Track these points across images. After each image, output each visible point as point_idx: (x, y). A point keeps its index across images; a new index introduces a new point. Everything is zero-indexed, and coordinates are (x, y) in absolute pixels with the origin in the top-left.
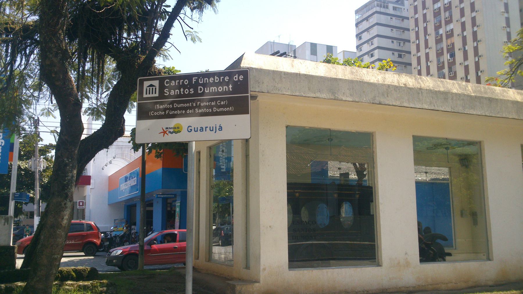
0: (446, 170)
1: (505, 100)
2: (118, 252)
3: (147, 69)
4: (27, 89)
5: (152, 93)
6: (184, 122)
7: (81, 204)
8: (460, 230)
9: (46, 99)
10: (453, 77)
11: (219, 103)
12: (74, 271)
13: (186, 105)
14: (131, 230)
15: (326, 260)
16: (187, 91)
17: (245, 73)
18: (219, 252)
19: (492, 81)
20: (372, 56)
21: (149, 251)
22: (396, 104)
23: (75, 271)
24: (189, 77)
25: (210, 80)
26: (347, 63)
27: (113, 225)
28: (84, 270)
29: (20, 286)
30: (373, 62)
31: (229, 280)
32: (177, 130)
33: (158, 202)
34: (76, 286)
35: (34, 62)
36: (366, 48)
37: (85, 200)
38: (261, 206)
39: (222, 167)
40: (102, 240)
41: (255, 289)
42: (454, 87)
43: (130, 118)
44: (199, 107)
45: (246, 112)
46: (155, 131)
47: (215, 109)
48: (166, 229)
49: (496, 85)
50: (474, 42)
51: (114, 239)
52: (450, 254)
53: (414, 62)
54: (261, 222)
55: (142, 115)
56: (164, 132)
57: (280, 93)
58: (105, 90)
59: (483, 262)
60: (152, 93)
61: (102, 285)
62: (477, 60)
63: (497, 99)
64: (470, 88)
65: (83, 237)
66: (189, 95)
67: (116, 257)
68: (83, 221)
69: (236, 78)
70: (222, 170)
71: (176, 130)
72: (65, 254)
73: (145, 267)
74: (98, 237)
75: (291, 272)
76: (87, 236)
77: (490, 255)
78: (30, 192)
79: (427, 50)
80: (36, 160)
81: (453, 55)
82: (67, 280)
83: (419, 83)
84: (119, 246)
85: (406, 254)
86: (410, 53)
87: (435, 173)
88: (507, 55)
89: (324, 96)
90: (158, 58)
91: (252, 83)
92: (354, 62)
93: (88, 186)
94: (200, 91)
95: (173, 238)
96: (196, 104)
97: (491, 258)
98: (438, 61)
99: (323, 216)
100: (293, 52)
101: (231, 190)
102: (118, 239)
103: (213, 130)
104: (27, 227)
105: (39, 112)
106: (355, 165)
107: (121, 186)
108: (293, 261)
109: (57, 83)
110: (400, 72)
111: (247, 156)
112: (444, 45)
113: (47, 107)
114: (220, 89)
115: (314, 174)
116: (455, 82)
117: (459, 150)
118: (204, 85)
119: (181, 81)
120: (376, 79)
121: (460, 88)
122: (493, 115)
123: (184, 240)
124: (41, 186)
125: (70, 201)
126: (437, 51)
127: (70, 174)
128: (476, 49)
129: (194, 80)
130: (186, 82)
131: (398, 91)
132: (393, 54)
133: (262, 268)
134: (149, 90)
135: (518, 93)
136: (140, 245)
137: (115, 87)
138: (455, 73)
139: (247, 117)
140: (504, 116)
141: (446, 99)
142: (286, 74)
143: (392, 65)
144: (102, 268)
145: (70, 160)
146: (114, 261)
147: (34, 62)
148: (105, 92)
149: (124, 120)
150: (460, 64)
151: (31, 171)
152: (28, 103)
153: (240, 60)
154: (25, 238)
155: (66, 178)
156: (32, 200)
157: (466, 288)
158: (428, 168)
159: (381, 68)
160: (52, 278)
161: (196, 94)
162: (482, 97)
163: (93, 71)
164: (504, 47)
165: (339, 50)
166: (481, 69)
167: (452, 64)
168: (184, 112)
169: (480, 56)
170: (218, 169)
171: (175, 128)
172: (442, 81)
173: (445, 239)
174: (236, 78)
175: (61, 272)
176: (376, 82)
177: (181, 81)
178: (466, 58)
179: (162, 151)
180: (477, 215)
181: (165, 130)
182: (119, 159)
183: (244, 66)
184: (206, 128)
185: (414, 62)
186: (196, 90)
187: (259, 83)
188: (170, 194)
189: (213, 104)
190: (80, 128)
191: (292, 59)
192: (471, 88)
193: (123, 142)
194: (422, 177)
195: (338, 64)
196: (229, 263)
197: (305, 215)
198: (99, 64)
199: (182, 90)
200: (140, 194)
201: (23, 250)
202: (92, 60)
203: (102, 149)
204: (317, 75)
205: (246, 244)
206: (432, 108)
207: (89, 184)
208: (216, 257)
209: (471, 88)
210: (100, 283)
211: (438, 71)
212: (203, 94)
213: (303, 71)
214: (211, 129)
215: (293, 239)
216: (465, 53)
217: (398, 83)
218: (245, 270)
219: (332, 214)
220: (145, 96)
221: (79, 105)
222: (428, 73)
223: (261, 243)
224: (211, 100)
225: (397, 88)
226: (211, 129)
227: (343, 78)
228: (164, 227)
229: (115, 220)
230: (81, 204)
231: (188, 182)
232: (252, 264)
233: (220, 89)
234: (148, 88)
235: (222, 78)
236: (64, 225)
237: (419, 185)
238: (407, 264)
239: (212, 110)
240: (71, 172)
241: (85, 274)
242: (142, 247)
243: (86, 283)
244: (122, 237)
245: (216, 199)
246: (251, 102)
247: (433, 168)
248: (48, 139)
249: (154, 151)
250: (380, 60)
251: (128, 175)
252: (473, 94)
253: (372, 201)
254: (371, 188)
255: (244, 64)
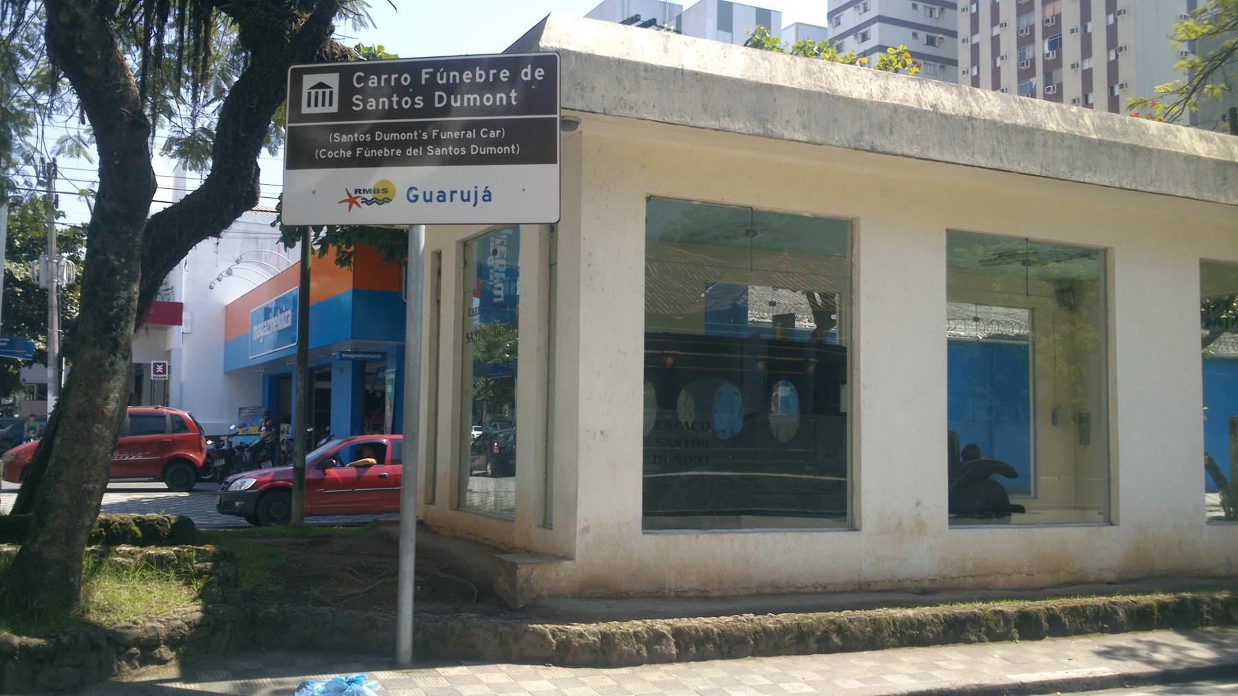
0: (1024, 314)
1: (1169, 153)
2: (246, 482)
3: (314, 44)
4: (22, 86)
5: (323, 105)
6: (399, 177)
7: (160, 368)
8: (1048, 453)
9: (66, 113)
10: (1057, 97)
11: (485, 133)
12: (137, 524)
13: (403, 136)
14: (278, 432)
15: (733, 513)
16: (406, 103)
17: (549, 62)
18: (483, 489)
19: (1144, 107)
20: (865, 38)
21: (319, 483)
22: (912, 153)
23: (141, 523)
24: (413, 67)
25: (464, 76)
26: (802, 50)
27: (236, 419)
28: (162, 523)
29: (7, 553)
30: (865, 54)
31: (504, 552)
32: (382, 196)
33: (342, 371)
34: (139, 556)
35: (36, 20)
36: (851, 18)
37: (169, 360)
38: (582, 382)
39: (496, 292)
40: (208, 456)
41: (562, 574)
42: (1048, 116)
43: (271, 166)
44: (437, 142)
45: (551, 159)
46: (332, 196)
47: (475, 149)
48: (363, 434)
49: (1151, 117)
50: (1108, 13)
51: (237, 453)
52: (1020, 509)
53: (964, 58)
54: (581, 422)
55: (297, 159)
56: (352, 201)
57: (635, 115)
58: (212, 96)
59: (1095, 529)
60: (323, 105)
61: (202, 556)
62: (1113, 57)
63: (1150, 150)
64: (1088, 121)
65: (163, 446)
66: (412, 112)
67: (241, 495)
68: (164, 410)
69: (526, 74)
70: (496, 300)
71: (380, 196)
72: (110, 486)
73: (309, 521)
74: (200, 449)
75: (647, 537)
76: (172, 444)
77: (1113, 513)
78: (36, 338)
79: (997, 30)
80: (51, 260)
81: (1056, 45)
82: (118, 544)
83: (967, 104)
84: (250, 470)
85: (918, 504)
86: (953, 34)
87: (998, 323)
88: (1184, 47)
89: (738, 126)
90: (343, 21)
91: (565, 88)
92: (819, 50)
93: (176, 327)
94: (440, 102)
95: (379, 451)
96: (430, 135)
97: (1113, 519)
98: (1021, 56)
99: (728, 415)
100: (674, 21)
101: (514, 350)
102: (247, 454)
103: (468, 200)
104: (32, 419)
105: (51, 145)
106: (810, 296)
107: (255, 328)
108: (655, 514)
109: (89, 71)
110: (922, 77)
111: (551, 266)
112: (1037, 18)
113: (73, 133)
114: (488, 100)
115: (713, 315)
116: (1053, 104)
117: (1056, 269)
118: (451, 89)
119: (393, 77)
120: (867, 91)
121: (1065, 119)
122: (1139, 188)
123: (398, 462)
124: (64, 324)
125: (125, 358)
126: (1020, 31)
127: (124, 294)
128: (1112, 32)
129: (424, 76)
130: (406, 79)
131: (917, 121)
132: (915, 35)
133: (580, 525)
134: (316, 98)
135: (1201, 137)
136: (296, 469)
137: (235, 89)
138: (1060, 86)
139: (551, 170)
140: (1164, 190)
141: (1029, 145)
142: (650, 69)
143: (909, 62)
144: (206, 514)
145: (123, 260)
146: (237, 504)
147: (36, 20)
148: (213, 101)
149: (258, 170)
150: (1073, 66)
151: (38, 286)
152: (24, 123)
153: (538, 30)
154: (25, 445)
155: (115, 303)
156: (41, 357)
157: (1052, 587)
158: (982, 308)
159: (885, 66)
160: (83, 537)
161: (429, 110)
162: (1115, 143)
163: (181, 49)
164: (1175, 25)
165: (786, 21)
166: (1121, 81)
167: (1053, 66)
168: (399, 152)
169: (1121, 49)
170: (485, 294)
171: (376, 191)
172: (1022, 102)
173: (1011, 473)
174: (526, 74)
175: (106, 524)
176: (864, 97)
177: (393, 77)
178: (1086, 52)
179: (352, 249)
180: (1088, 423)
181: (354, 195)
182: (250, 266)
183: (549, 45)
184: (452, 193)
185: (964, 58)
186: (429, 100)
187: (583, 88)
188: (371, 353)
189: (470, 135)
190: (148, 185)
191: (673, 35)
192: (1090, 122)
193: (256, 222)
194: (966, 331)
195: (781, 51)
196: (506, 516)
197: (686, 409)
198: (197, 32)
199: (395, 99)
200: (296, 351)
201: (19, 472)
202: (180, 23)
203: (206, 237)
204: (724, 74)
205: (546, 472)
206: (996, 166)
207: (179, 322)
208: (475, 500)
209: (1090, 122)
210: (198, 551)
211: (1019, 81)
212: (447, 110)
213: (691, 65)
214: (465, 197)
215: (655, 462)
216: (1086, 40)
217: (919, 101)
218: (542, 530)
219: (748, 406)
220: (305, 110)
221: (144, 130)
222: (996, 85)
223: (581, 470)
224: (468, 126)
225: (914, 114)
226: (465, 197)
227: (788, 84)
228: (358, 428)
229: (240, 409)
230: (160, 368)
231: (408, 321)
232: (558, 515)
233: (488, 100)
234: (313, 92)
235: (492, 72)
236: (110, 414)
237: (956, 348)
238: (920, 528)
239: (468, 150)
240: (127, 288)
241: (165, 531)
242: (300, 471)
243: (164, 551)
244: (256, 449)
245: (480, 368)
246: (561, 135)
247: (995, 309)
248: (76, 213)
249: (332, 249)
250: (882, 49)
251: (271, 303)
252: (1094, 137)
253: (845, 382)
254: (845, 349)
255: (548, 41)
